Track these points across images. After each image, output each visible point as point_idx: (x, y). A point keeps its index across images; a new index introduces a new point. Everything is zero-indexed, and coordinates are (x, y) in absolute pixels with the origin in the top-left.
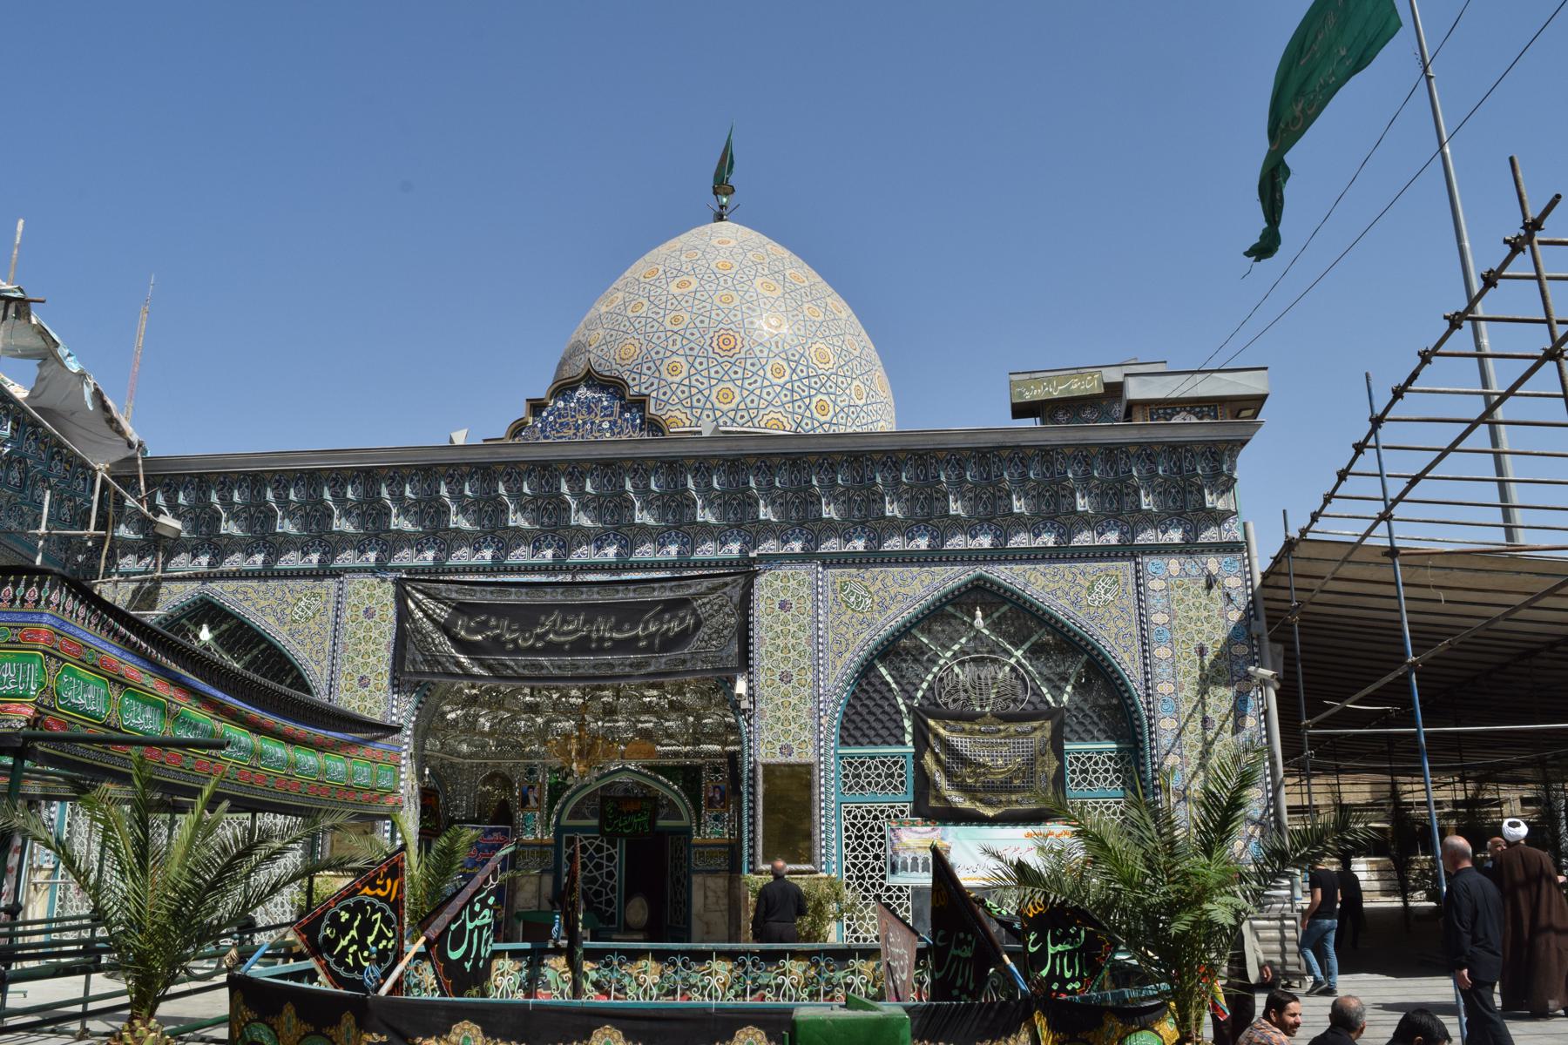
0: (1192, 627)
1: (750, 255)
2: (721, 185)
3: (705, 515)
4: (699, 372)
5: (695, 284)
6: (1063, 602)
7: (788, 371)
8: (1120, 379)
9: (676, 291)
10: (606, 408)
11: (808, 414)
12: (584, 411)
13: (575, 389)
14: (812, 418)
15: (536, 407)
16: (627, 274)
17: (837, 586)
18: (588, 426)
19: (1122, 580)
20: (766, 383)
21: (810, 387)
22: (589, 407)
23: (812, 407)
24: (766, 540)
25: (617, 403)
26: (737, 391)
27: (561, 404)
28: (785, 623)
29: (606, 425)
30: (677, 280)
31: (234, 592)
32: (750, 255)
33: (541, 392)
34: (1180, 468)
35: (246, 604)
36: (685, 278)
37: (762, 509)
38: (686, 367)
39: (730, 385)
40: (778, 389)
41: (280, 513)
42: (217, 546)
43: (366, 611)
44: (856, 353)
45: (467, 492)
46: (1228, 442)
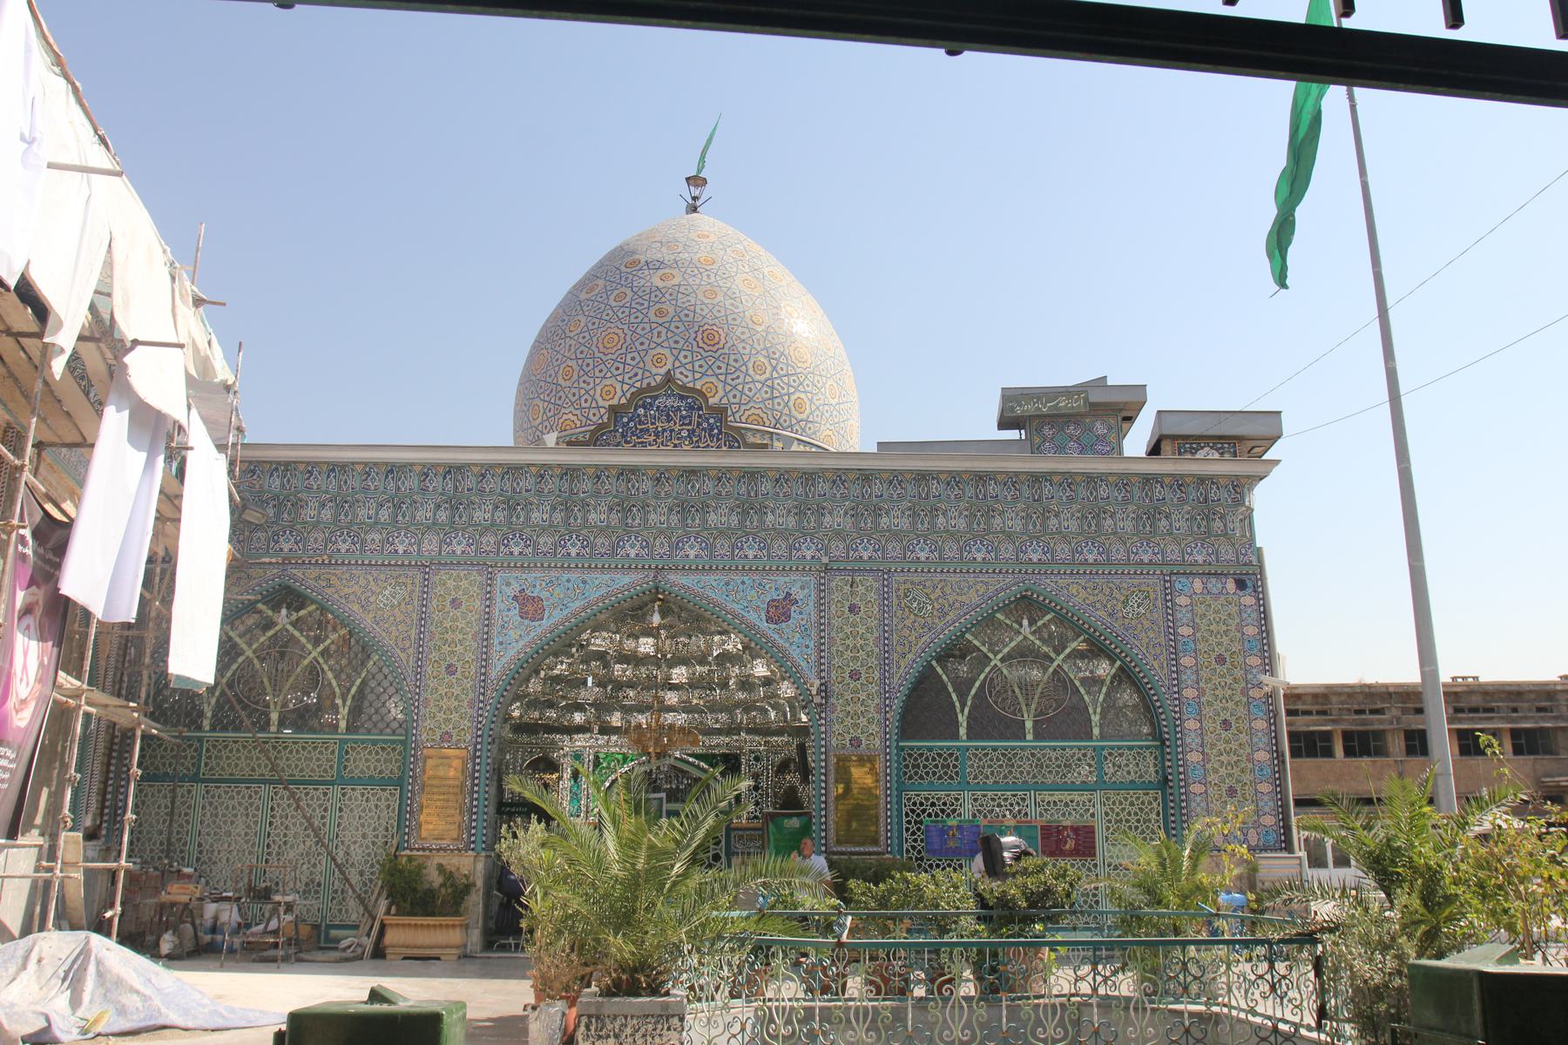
0: (1212, 640)
4: (683, 365)
7: (769, 369)
17: (901, 593)
19: (1152, 596)
22: (668, 416)
26: (720, 386)
28: (854, 625)
29: (685, 434)
31: (318, 578)
35: (329, 591)
38: (671, 359)
43: (454, 601)
46: (1248, 477)
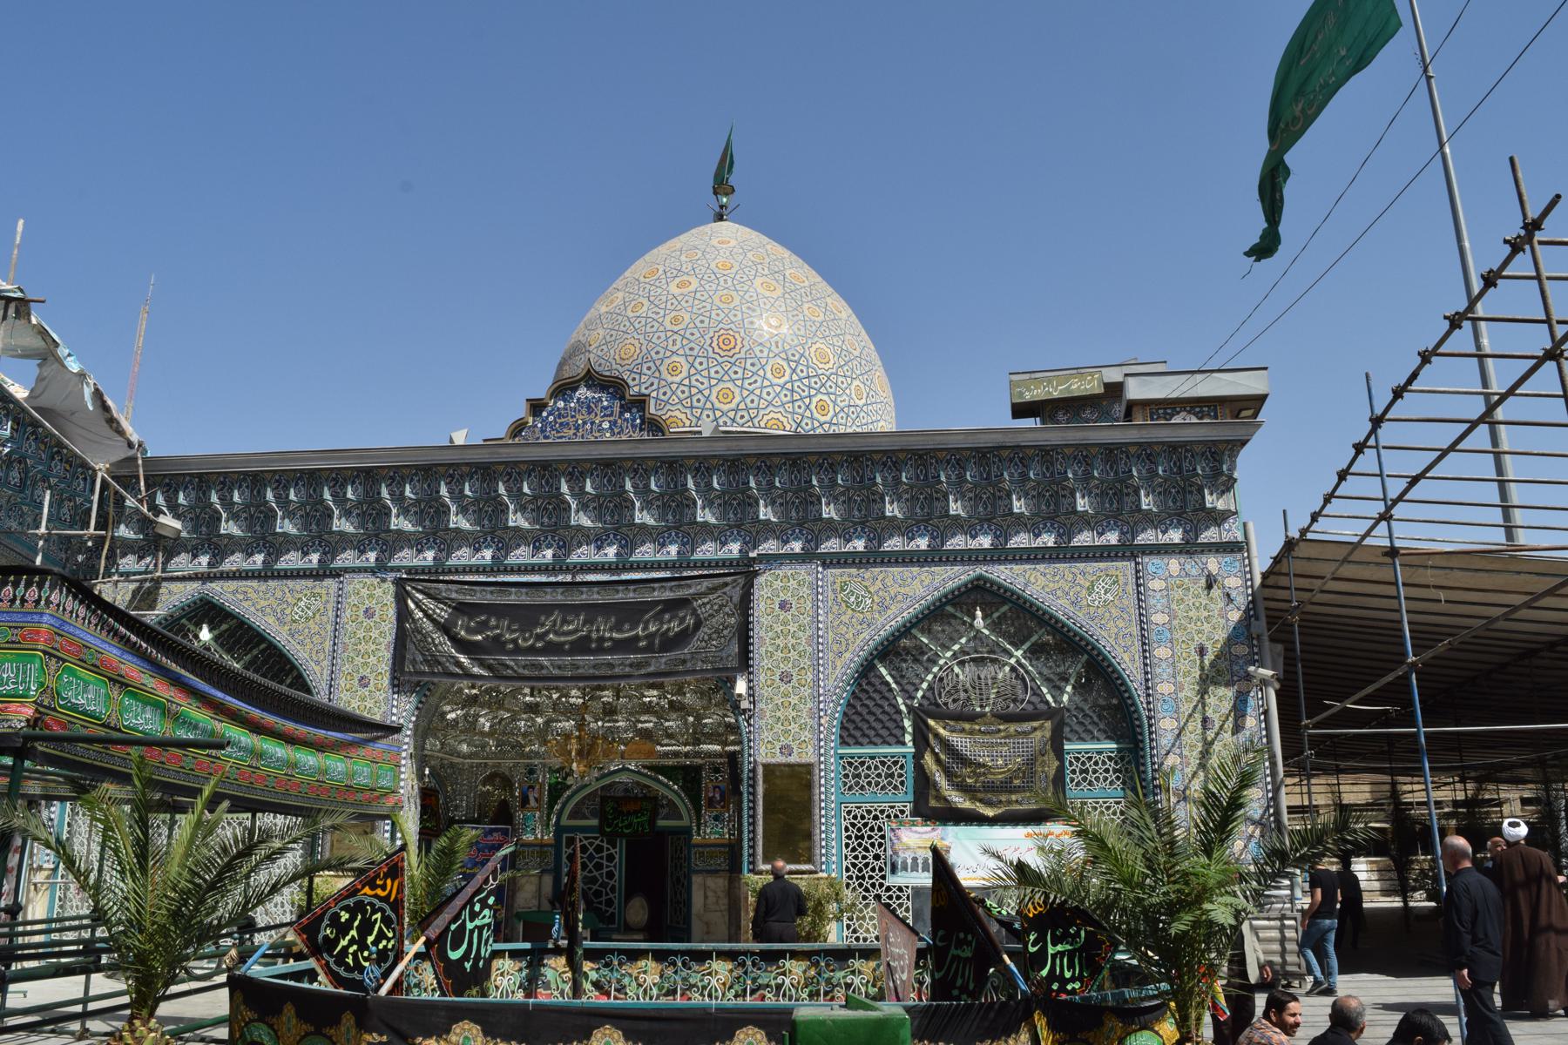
0: (1192, 627)
1: (750, 255)
2: (721, 185)
3: (705, 515)
4: (699, 372)
5: (695, 284)
6: (1063, 602)
7: (788, 371)
8: (1120, 379)
9: (676, 291)
10: (606, 408)
11: (808, 414)
12: (584, 411)
13: (575, 389)
14: (812, 418)
15: (536, 407)
16: (627, 274)
17: (837, 586)
18: (588, 426)
19: (1122, 580)
20: (766, 383)
21: (810, 387)
22: (589, 407)
23: (812, 407)
24: (766, 540)
25: (617, 403)
26: (737, 391)
27: (561, 404)
28: (785, 623)
29: (606, 425)
30: (677, 280)
31: (234, 592)
32: (750, 255)
33: (541, 392)
34: (1180, 468)
35: (246, 604)
36: (685, 278)
37: (762, 509)
38: (686, 367)
39: (730, 385)
40: (778, 389)
41: (280, 513)
42: (217, 546)
43: (366, 611)
44: (856, 353)
45: (467, 492)
46: (1228, 442)
